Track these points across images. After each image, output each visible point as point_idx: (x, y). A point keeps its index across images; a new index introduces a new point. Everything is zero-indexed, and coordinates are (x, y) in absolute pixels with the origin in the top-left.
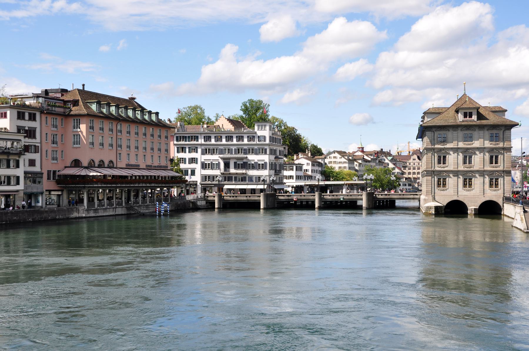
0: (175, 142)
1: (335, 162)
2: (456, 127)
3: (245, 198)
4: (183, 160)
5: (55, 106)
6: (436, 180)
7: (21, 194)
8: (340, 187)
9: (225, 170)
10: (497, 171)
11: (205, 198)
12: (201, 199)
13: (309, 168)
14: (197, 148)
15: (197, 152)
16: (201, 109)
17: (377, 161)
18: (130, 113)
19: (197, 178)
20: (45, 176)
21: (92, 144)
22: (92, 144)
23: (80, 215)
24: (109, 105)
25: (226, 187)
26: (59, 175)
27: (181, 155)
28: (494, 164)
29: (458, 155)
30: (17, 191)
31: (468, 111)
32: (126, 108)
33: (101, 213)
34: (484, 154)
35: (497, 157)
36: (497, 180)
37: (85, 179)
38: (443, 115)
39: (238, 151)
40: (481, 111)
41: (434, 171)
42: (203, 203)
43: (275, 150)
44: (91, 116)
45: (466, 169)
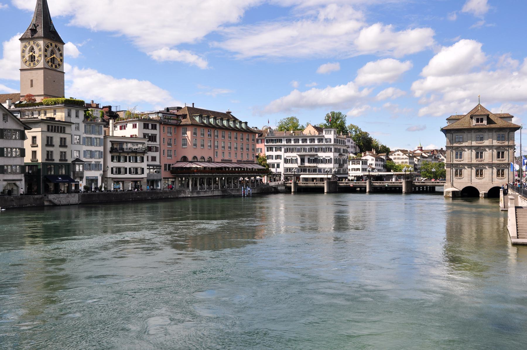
0: (266, 144)
1: (398, 158)
2: (470, 130)
3: (313, 185)
4: (271, 157)
5: (170, 119)
6: (454, 170)
7: (145, 180)
8: (390, 177)
9: (301, 164)
10: (503, 164)
11: (284, 184)
12: (281, 185)
13: (374, 162)
14: (281, 148)
15: (281, 151)
16: (296, 119)
17: (433, 158)
18: (225, 123)
19: (281, 170)
20: (163, 168)
21: (230, 148)
22: (195, 145)
23: (186, 196)
24: (208, 117)
25: (302, 176)
26: (172, 168)
27: (270, 153)
28: (501, 159)
29: (472, 151)
30: (142, 178)
31: (480, 117)
32: (222, 120)
33: (202, 194)
34: (493, 151)
35: (503, 153)
36: (503, 171)
37: (189, 170)
38: (461, 121)
39: (310, 150)
40: (491, 117)
41: (452, 164)
42: (283, 188)
43: (339, 150)
44: (194, 125)
45: (478, 162)
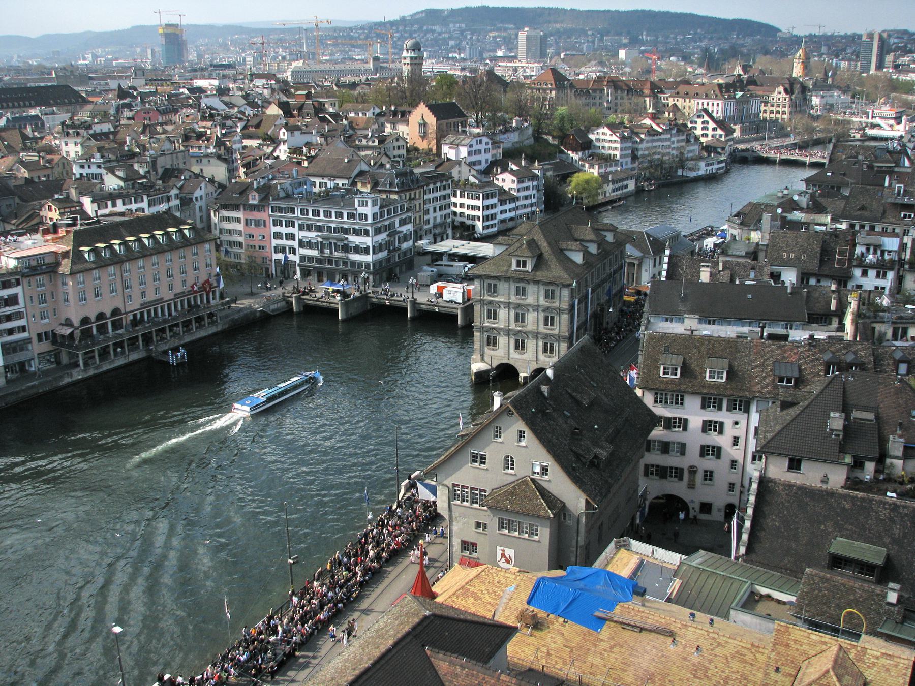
1: (604, 140)
23: (74, 379)
